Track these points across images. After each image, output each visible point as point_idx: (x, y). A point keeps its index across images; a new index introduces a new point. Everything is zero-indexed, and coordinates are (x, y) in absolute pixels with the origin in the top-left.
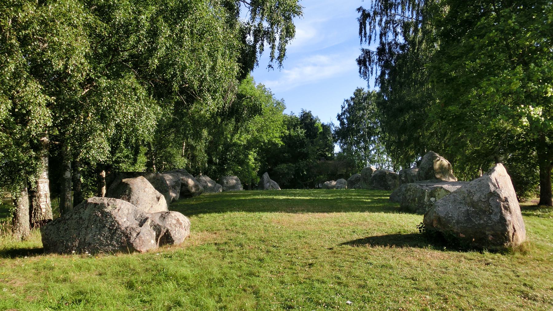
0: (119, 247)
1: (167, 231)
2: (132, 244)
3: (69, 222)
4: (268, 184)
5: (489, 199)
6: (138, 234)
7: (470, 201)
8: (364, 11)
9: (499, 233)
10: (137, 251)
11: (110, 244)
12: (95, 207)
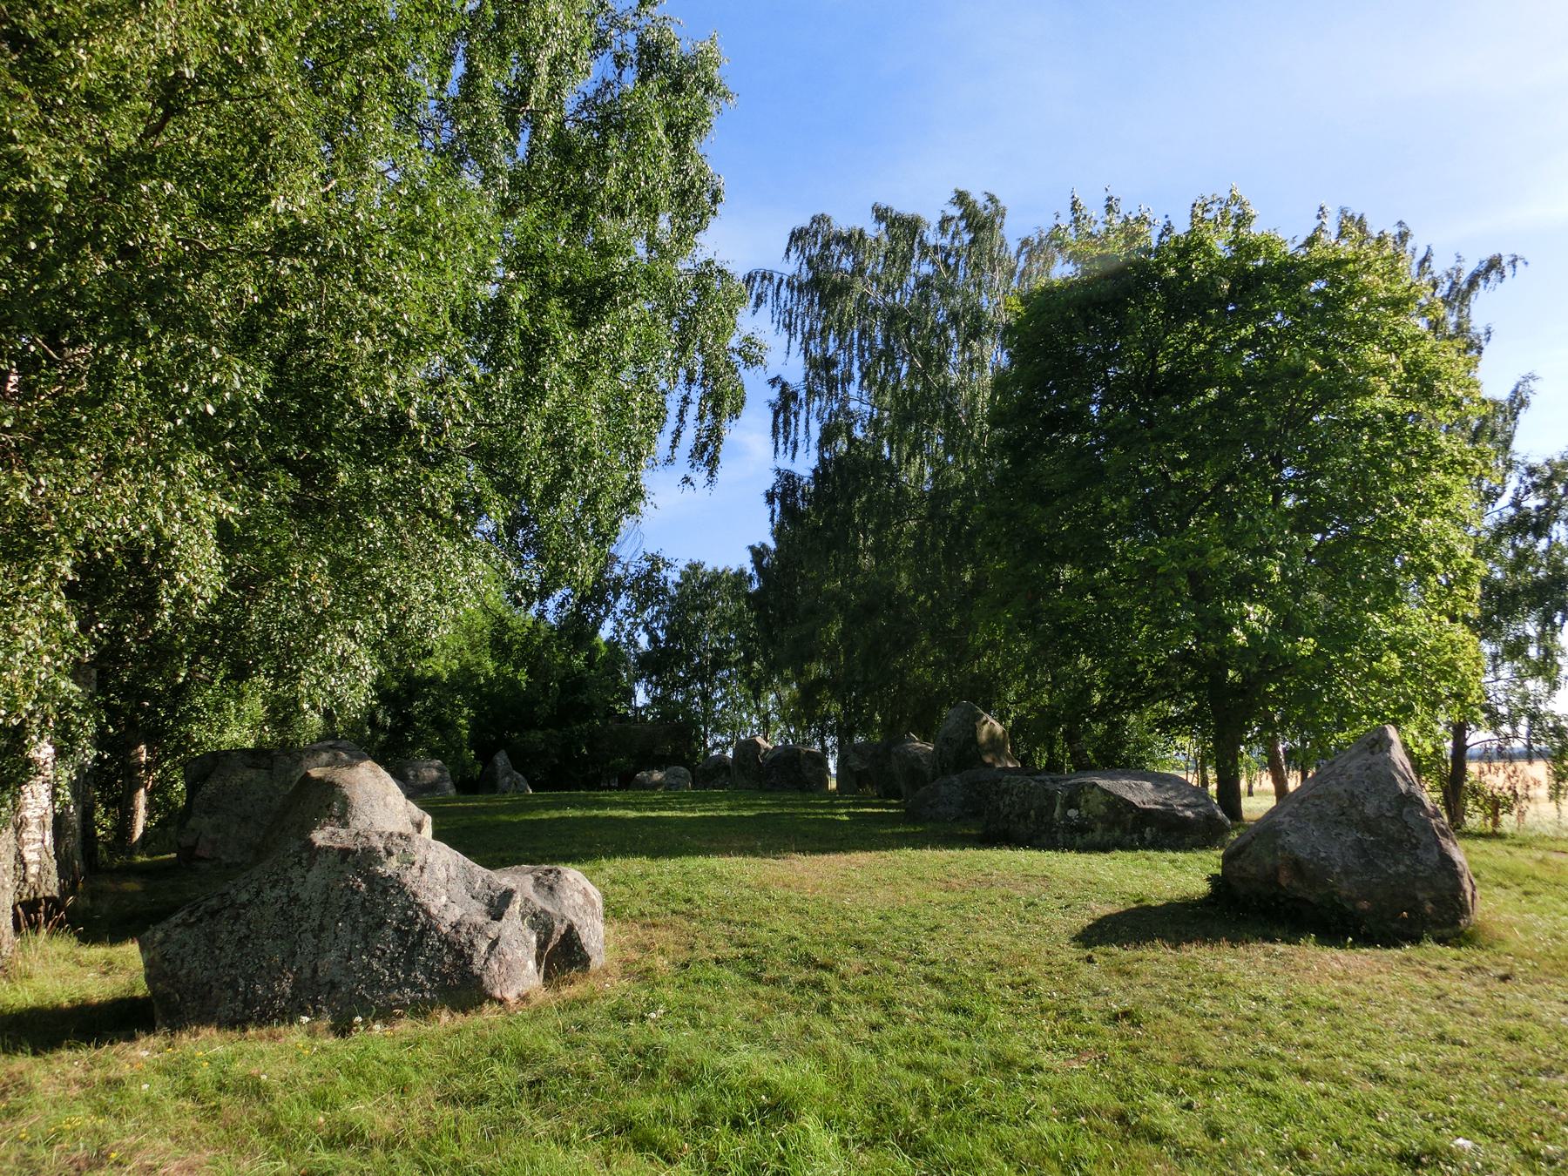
0: (436, 990)
1: (571, 928)
2: (479, 978)
3: (252, 913)
6: (494, 944)
8: (784, 385)
9: (1447, 893)
10: (492, 999)
11: (406, 983)
12: (344, 860)
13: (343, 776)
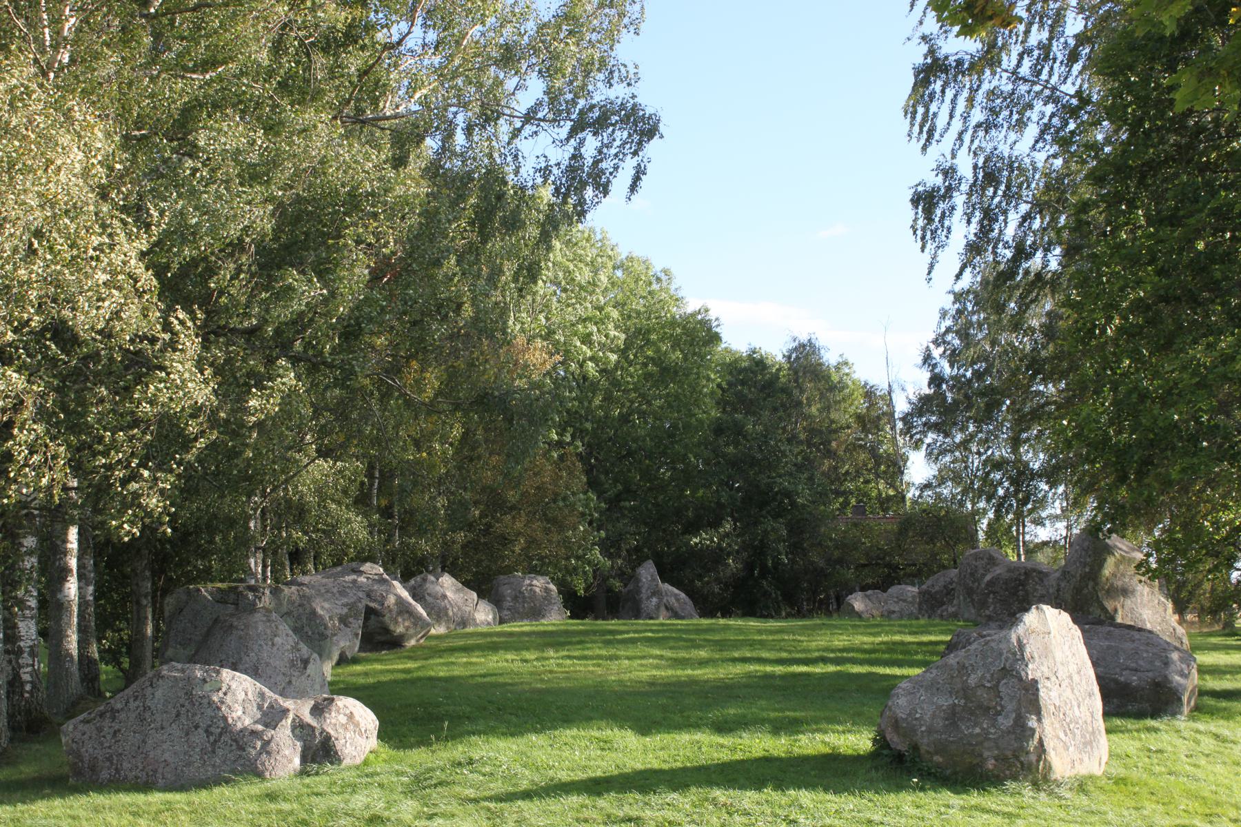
4: (654, 600)
5: (999, 682)
7: (959, 686)
9: (1009, 753)
13: (1139, 587)
